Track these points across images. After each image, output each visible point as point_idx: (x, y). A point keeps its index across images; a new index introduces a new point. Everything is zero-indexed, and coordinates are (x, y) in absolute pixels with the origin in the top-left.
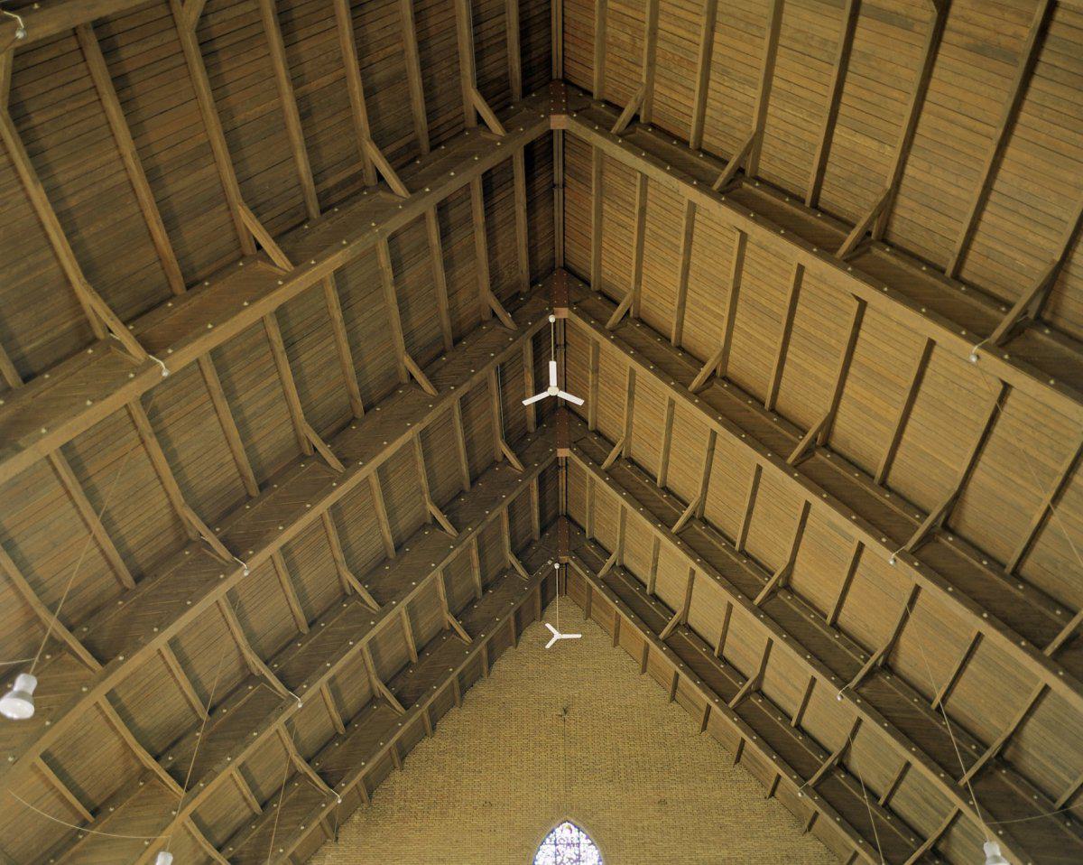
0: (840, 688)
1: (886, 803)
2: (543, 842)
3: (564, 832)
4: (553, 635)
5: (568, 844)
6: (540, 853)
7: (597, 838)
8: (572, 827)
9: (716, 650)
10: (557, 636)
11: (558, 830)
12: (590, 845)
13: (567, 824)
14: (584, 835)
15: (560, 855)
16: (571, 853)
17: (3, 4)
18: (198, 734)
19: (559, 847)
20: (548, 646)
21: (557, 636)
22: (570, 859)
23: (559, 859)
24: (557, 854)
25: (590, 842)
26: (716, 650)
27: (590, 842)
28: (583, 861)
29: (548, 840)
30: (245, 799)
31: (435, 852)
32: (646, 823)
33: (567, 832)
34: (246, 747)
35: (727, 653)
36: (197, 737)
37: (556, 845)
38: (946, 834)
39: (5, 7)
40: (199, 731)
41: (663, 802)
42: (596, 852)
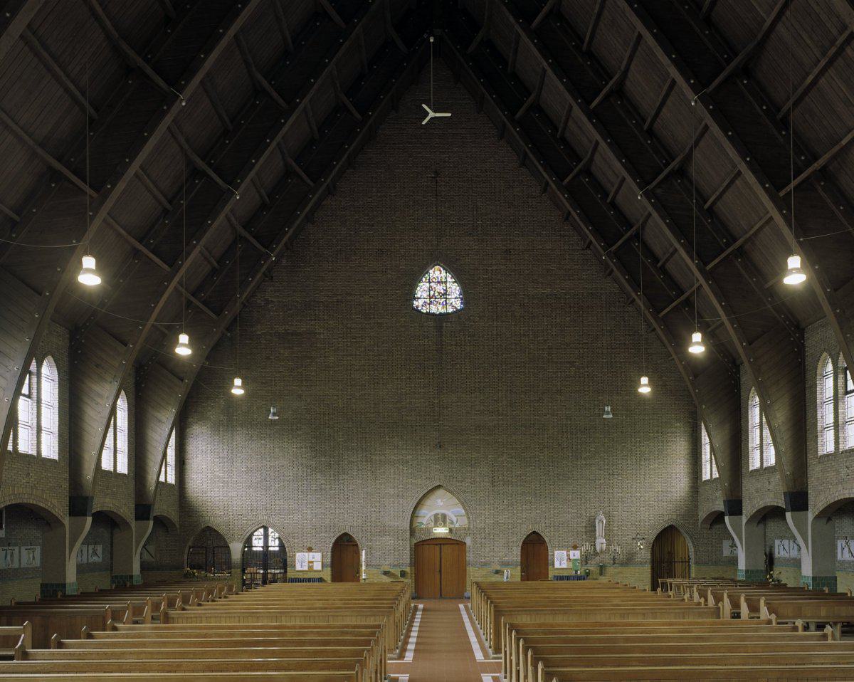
0: (641, 189)
1: (663, 266)
2: (421, 281)
3: (436, 273)
4: (428, 114)
5: (438, 282)
6: (418, 288)
7: (459, 279)
8: (442, 269)
9: (610, 197)
10: (432, 114)
11: (431, 271)
12: (453, 282)
13: (437, 267)
14: (450, 276)
15: (432, 290)
16: (440, 288)
17: (852, 680)
18: (182, 202)
19: (432, 284)
20: (424, 123)
21: (432, 114)
22: (439, 293)
23: (432, 293)
24: (430, 289)
25: (453, 280)
26: (610, 197)
27: (453, 280)
28: (449, 295)
29: (424, 279)
30: (206, 258)
31: (343, 288)
32: (495, 268)
33: (437, 273)
34: (205, 232)
35: (619, 199)
36: (182, 204)
37: (430, 282)
38: (667, 260)
39: (846, 674)
40: (182, 200)
41: (508, 251)
42: (458, 288)
